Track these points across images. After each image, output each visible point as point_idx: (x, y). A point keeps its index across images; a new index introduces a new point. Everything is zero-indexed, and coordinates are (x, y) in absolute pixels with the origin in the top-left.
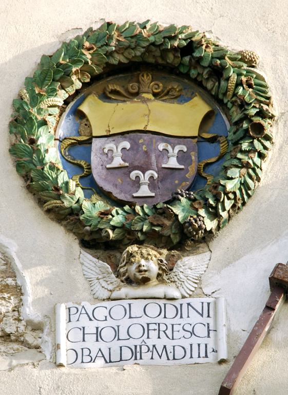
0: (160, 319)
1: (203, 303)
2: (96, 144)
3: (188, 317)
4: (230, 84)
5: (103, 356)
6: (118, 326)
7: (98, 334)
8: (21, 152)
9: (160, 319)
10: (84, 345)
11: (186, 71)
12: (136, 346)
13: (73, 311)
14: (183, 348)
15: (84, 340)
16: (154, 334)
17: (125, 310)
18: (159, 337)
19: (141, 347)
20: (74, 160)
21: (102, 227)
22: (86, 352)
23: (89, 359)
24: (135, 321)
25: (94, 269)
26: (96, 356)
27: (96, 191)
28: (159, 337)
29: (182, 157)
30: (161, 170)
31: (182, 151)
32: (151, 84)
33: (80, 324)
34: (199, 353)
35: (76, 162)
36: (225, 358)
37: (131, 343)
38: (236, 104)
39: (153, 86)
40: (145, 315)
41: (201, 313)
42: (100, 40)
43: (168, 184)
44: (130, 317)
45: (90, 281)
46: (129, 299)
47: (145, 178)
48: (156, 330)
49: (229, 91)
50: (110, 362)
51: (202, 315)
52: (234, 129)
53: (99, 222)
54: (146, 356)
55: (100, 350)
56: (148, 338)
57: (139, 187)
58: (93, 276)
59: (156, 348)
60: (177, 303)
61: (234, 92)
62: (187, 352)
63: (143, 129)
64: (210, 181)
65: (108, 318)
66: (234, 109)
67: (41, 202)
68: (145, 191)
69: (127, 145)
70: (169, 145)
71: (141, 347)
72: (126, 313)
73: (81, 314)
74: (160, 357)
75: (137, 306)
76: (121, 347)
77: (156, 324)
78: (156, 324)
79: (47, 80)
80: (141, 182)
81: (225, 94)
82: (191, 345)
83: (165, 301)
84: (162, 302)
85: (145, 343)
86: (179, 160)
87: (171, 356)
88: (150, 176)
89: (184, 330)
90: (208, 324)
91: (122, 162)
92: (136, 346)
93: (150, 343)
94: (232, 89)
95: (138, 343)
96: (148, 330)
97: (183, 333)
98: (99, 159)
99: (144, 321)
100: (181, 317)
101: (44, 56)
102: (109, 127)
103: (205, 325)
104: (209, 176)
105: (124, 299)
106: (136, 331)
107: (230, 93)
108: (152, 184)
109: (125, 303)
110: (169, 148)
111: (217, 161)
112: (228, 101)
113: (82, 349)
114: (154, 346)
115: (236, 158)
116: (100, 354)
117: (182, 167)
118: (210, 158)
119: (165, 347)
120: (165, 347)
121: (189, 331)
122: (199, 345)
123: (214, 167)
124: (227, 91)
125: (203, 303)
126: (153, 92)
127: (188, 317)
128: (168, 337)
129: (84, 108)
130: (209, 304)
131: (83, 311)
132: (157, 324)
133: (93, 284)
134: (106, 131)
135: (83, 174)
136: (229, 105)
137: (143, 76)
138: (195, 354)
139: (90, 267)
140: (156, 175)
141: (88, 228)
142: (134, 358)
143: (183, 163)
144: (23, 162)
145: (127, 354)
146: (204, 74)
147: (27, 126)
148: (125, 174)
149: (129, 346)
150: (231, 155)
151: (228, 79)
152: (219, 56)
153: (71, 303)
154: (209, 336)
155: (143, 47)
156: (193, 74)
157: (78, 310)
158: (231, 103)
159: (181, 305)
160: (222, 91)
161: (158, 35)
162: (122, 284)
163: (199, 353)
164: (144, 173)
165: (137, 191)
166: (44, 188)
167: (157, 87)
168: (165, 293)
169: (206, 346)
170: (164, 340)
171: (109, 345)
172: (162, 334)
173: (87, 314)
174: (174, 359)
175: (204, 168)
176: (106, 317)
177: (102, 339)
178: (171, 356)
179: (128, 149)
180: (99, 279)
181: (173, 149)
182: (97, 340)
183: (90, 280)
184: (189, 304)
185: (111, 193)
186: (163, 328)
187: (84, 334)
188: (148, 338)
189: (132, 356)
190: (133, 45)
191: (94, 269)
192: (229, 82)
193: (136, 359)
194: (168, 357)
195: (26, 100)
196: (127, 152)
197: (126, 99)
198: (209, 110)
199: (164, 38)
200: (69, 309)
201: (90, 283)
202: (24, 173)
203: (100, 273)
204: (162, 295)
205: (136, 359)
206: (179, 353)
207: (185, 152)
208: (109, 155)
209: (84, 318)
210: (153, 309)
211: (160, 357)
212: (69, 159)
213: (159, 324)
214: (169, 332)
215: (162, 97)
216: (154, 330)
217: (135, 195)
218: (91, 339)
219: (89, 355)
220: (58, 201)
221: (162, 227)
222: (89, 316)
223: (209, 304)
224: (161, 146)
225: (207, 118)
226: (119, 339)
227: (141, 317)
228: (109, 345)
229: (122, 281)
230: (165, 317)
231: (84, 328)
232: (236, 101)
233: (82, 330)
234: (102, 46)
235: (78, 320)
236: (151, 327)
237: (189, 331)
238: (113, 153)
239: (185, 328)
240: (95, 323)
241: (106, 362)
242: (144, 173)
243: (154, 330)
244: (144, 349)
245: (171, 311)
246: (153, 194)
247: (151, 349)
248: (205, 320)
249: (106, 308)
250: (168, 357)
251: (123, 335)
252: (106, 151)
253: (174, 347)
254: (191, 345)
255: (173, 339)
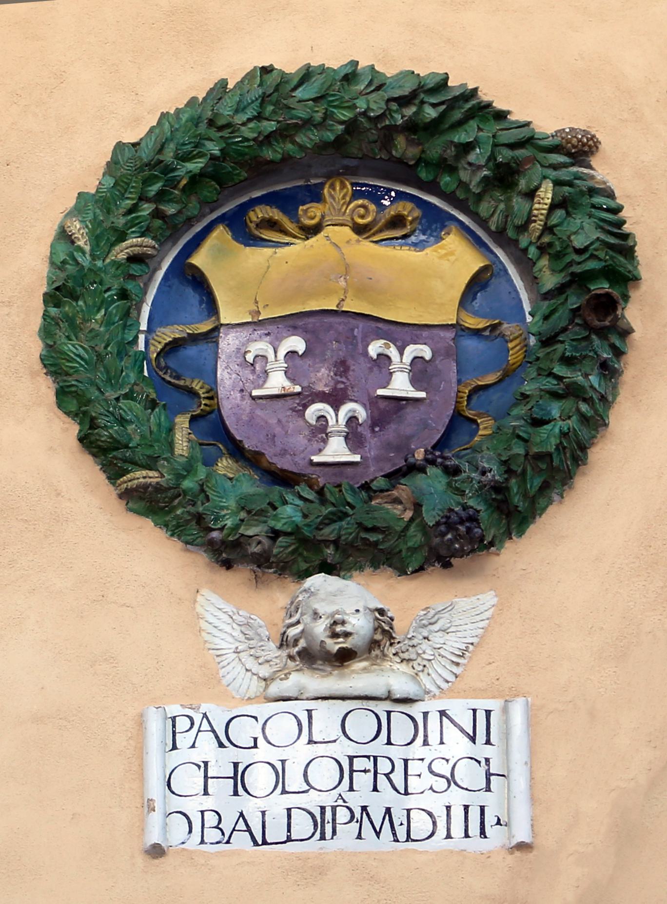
0: (378, 747)
1: (474, 711)
2: (228, 342)
3: (442, 743)
4: (537, 206)
5: (249, 830)
6: (283, 762)
7: (238, 779)
8: (68, 361)
9: (378, 747)
10: (208, 803)
11: (431, 178)
12: (323, 809)
13: (182, 724)
14: (430, 814)
15: (206, 793)
16: (363, 781)
17: (300, 724)
18: (375, 789)
19: (334, 809)
20: (178, 378)
21: (250, 533)
22: (211, 819)
23: (215, 835)
24: (320, 749)
25: (228, 629)
26: (234, 830)
27: (228, 450)
28: (375, 789)
29: (419, 372)
30: (372, 403)
31: (422, 358)
32: (352, 206)
33: (197, 756)
34: (466, 827)
35: (182, 383)
36: (527, 839)
37: (313, 801)
38: (551, 251)
39: (353, 210)
40: (343, 738)
41: (444, 718)
42: (245, 108)
43: (391, 432)
44: (311, 742)
45: (218, 656)
46: (308, 699)
47: (337, 419)
48: (369, 771)
49: (535, 221)
50: (265, 842)
51: (473, 739)
52: (545, 306)
53: (242, 520)
54: (347, 832)
55: (242, 815)
56: (351, 789)
57: (325, 441)
58: (224, 645)
59: (368, 815)
60: (416, 710)
61: (546, 224)
62: (438, 824)
63: (335, 308)
64: (485, 428)
65: (261, 742)
66: (544, 262)
67: (114, 472)
68: (336, 450)
69: (297, 343)
70: (392, 345)
71: (334, 809)
72: (300, 730)
73: (199, 731)
74: (378, 834)
75: (326, 717)
76: (289, 810)
77: (368, 757)
78: (368, 757)
79: (128, 198)
80: (329, 430)
81: (523, 228)
82: (448, 808)
83: (388, 706)
84: (381, 708)
85: (344, 801)
86: (416, 381)
87: (401, 833)
88: (350, 415)
89: (432, 772)
90: (487, 760)
91: (287, 384)
92: (323, 809)
93: (355, 801)
94: (542, 217)
95: (328, 800)
96: (352, 771)
97: (429, 780)
98: (234, 376)
99: (343, 749)
100: (426, 743)
101: (120, 146)
102: (257, 302)
103: (479, 762)
104: (480, 415)
105: (297, 699)
106: (325, 774)
107: (537, 226)
108: (353, 436)
109: (299, 708)
110: (393, 352)
111: (500, 381)
112: (531, 243)
113: (202, 812)
114: (364, 808)
115: (551, 374)
116: (241, 825)
117: (422, 395)
118: (486, 372)
119: (388, 811)
120: (388, 811)
121: (443, 777)
122: (466, 808)
123: (494, 396)
124: (529, 220)
125: (474, 711)
126: (355, 223)
127: (442, 743)
128: (399, 793)
129: (199, 260)
130: (488, 713)
131: (205, 726)
132: (372, 758)
133: (225, 663)
134: (251, 313)
135: (198, 412)
136: (533, 252)
137: (332, 187)
138: (457, 830)
139: (217, 623)
140: (362, 414)
141: (215, 534)
142: (318, 835)
143: (425, 385)
144: (73, 383)
145: (302, 825)
146: (473, 183)
147: (85, 302)
148: (293, 410)
149: (308, 808)
150: (539, 369)
151: (531, 194)
152: (512, 141)
153: (178, 707)
154: (488, 789)
155: (342, 123)
156: (447, 184)
157: (192, 724)
158: (538, 248)
159: (426, 714)
160: (518, 222)
161: (374, 95)
162: (291, 664)
163: (466, 827)
164: (336, 409)
165: (320, 450)
166: (118, 442)
167: (362, 211)
168: (388, 685)
169: (482, 809)
170: (387, 796)
171: (262, 804)
172: (382, 780)
173: (213, 731)
174: (408, 838)
175: (469, 397)
176: (255, 739)
177: (246, 790)
178: (401, 833)
179: (300, 353)
180: (239, 653)
181: (401, 354)
182: (236, 793)
183: (219, 652)
184: (443, 713)
185: (263, 454)
186: (384, 766)
187: (206, 777)
188: (351, 789)
189: (315, 830)
190: (318, 117)
191: (228, 629)
192: (536, 200)
193: (323, 837)
194: (394, 834)
195: (81, 243)
196: (298, 362)
197: (287, 239)
198: (482, 265)
199: (389, 100)
200: (174, 719)
201: (219, 659)
202: (73, 408)
203: (242, 637)
204: (381, 692)
205: (323, 837)
206: (421, 824)
207: (427, 362)
208: (258, 367)
209: (207, 741)
210: (362, 724)
211: (378, 834)
212: (168, 378)
213: (375, 758)
214: (398, 778)
215: (374, 234)
216: (365, 771)
217: (316, 459)
218: (221, 789)
219: (217, 827)
220: (151, 473)
221: (383, 532)
222: (217, 737)
223: (488, 713)
224: (375, 348)
225: (477, 284)
226: (284, 792)
227: (335, 741)
228: (262, 804)
229: (291, 657)
230: (389, 743)
231: (206, 764)
232: (550, 245)
233: (202, 769)
234: (249, 120)
235: (193, 746)
236: (358, 764)
237: (443, 777)
238: (267, 363)
239: (434, 767)
240: (232, 754)
241: (256, 843)
242: (336, 409)
243: (365, 771)
244: (343, 815)
245: (401, 729)
246: (357, 458)
247: (358, 815)
248: (482, 751)
249: (256, 718)
250: (394, 834)
251: (294, 782)
252: (250, 358)
253: (409, 811)
254: (448, 808)
255: (406, 793)
